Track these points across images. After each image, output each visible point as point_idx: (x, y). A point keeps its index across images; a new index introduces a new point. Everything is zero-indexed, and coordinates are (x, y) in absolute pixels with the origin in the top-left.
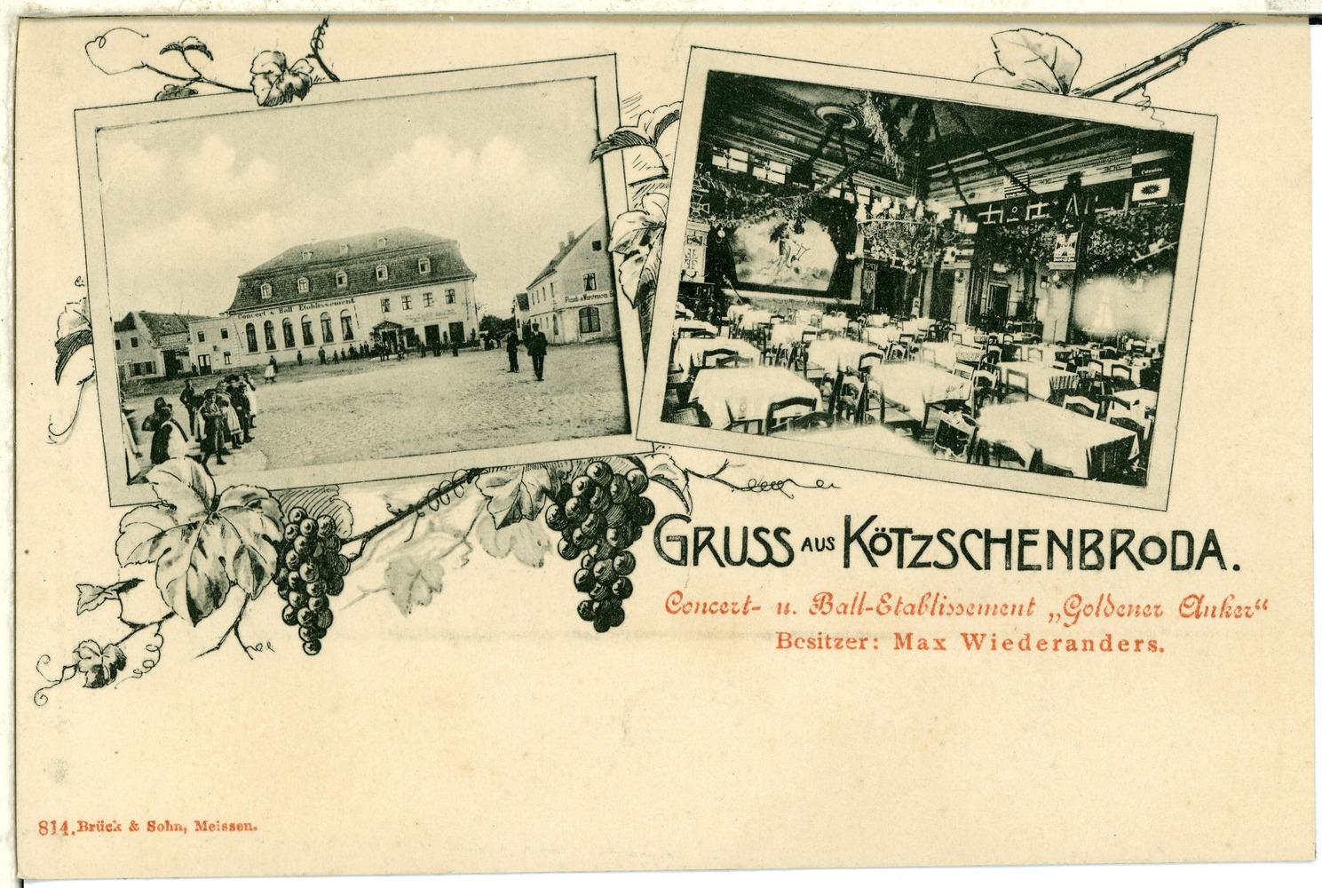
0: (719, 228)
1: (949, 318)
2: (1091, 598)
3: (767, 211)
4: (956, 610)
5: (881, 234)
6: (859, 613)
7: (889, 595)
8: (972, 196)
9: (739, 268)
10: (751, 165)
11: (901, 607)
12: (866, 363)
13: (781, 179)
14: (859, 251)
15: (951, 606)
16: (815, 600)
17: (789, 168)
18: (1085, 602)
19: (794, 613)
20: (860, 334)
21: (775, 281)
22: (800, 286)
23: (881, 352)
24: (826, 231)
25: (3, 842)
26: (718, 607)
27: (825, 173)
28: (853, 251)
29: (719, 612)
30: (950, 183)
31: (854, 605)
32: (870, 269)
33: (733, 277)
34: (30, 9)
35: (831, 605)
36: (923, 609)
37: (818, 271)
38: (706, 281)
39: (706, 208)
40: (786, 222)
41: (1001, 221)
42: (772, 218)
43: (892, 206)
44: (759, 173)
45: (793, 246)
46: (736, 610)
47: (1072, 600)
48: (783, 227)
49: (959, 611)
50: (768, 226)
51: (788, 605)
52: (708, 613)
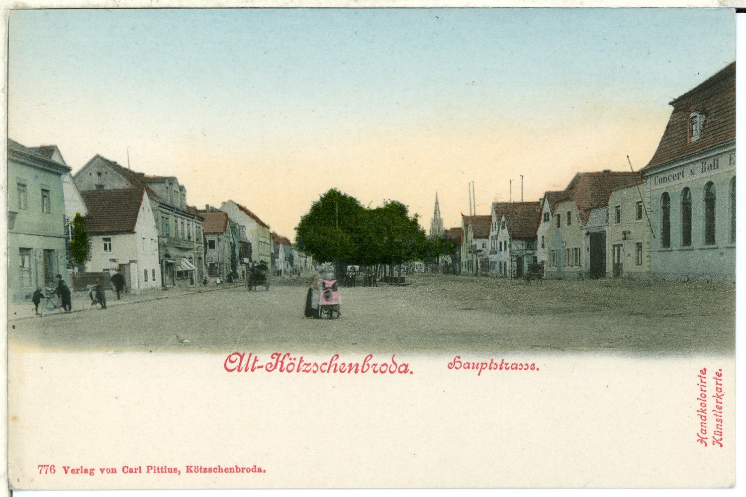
25: (2, 478)
29: (379, 372)
34: (17, 5)
46: (376, 370)
52: (338, 372)
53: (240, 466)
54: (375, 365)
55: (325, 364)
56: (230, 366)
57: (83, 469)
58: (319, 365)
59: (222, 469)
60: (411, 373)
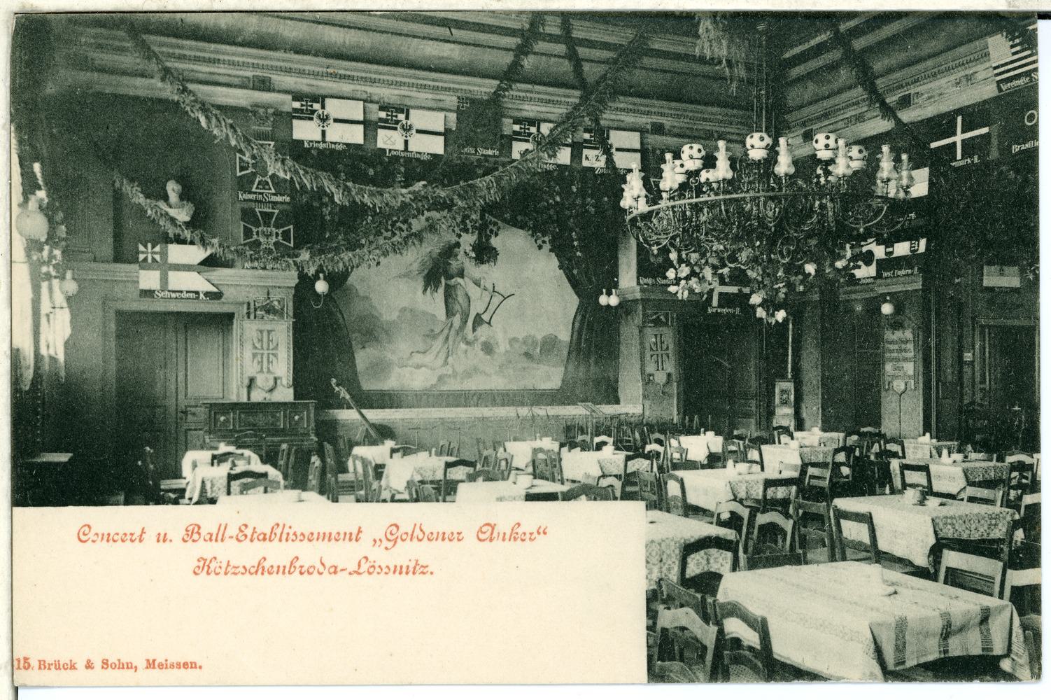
0: (316, 278)
1: (877, 423)
2: (406, 527)
3: (414, 222)
4: (299, 538)
5: (690, 236)
6: (222, 540)
7: (246, 526)
8: (906, 102)
9: (362, 358)
10: (370, 126)
11: (255, 536)
12: (696, 565)
13: (436, 146)
14: (628, 278)
15: (295, 534)
16: (187, 530)
17: (453, 117)
18: (402, 530)
19: (171, 541)
20: (660, 486)
21: (441, 379)
22: (497, 383)
23: (729, 534)
24: (547, 247)
26: (119, 537)
27: (531, 115)
28: (611, 284)
30: (845, 75)
31: (217, 534)
32: (657, 323)
33: (351, 382)
35: (199, 534)
36: (273, 536)
37: (534, 343)
38: (296, 397)
39: (286, 235)
40: (454, 239)
41: (994, 154)
42: (428, 236)
43: (709, 162)
44: (389, 140)
45: (474, 291)
46: (303, 571)
47: (391, 528)
48: (450, 251)
49: (302, 538)
50: (415, 257)
51: (165, 534)
53: (124, 660)
54: (301, 567)
55: (254, 567)
56: (482, 536)
57: (168, 662)
58: (248, 568)
59: (123, 664)
60: (432, 573)
